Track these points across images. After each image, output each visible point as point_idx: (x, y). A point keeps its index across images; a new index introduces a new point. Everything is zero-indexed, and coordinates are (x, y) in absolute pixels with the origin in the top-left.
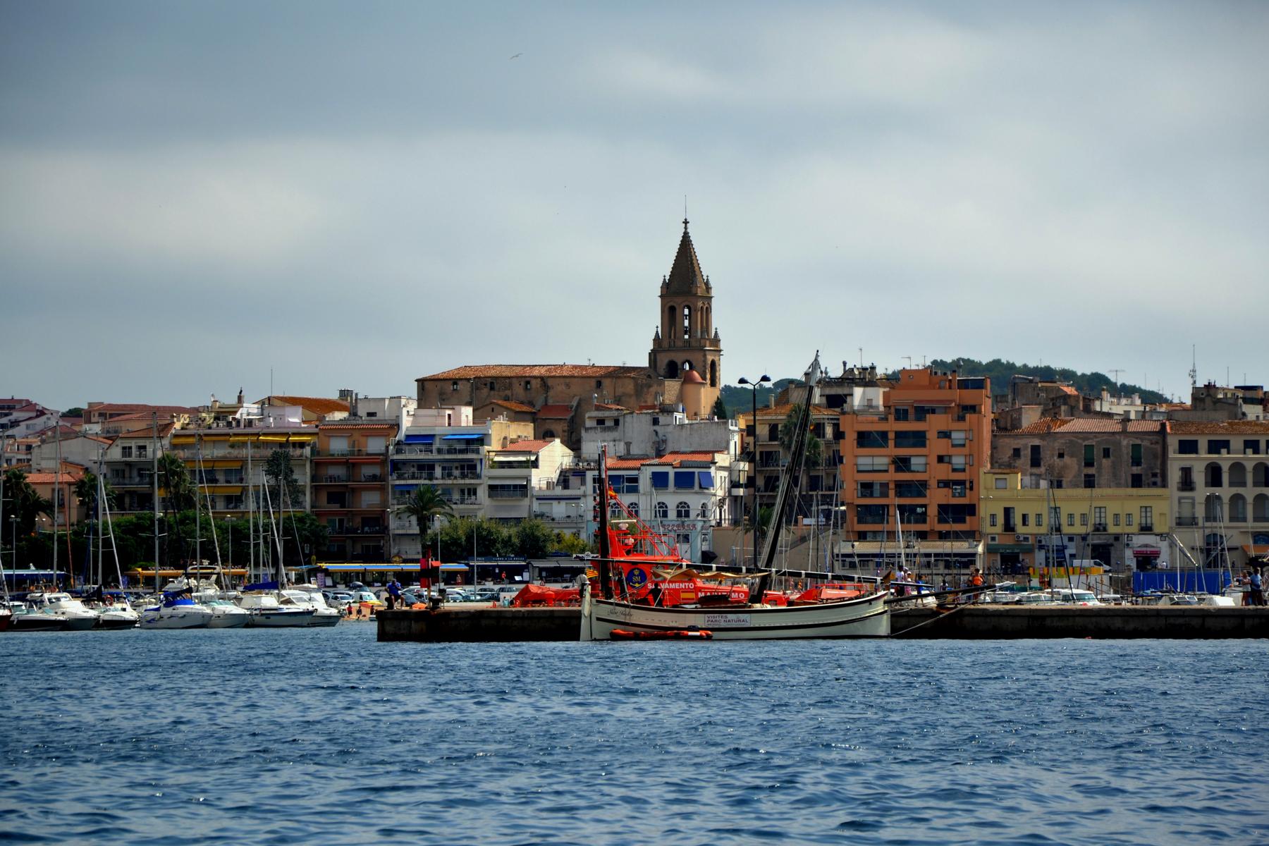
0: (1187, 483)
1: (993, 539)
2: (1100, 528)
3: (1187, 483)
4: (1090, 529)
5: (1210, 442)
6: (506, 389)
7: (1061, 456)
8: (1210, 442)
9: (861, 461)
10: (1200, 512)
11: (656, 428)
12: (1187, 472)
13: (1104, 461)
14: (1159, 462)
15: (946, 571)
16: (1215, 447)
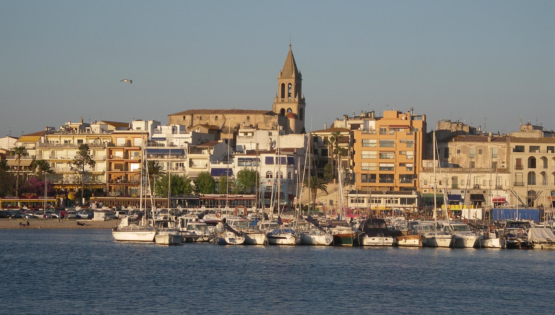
0: (519, 166)
1: (425, 191)
2: (477, 187)
3: (519, 166)
4: (472, 187)
5: (266, 157)
6: (207, 119)
7: (459, 152)
8: (266, 157)
9: (363, 153)
10: (526, 180)
11: (270, 137)
12: (519, 161)
13: (479, 155)
14: (505, 156)
15: (401, 206)
16: (532, 149)
